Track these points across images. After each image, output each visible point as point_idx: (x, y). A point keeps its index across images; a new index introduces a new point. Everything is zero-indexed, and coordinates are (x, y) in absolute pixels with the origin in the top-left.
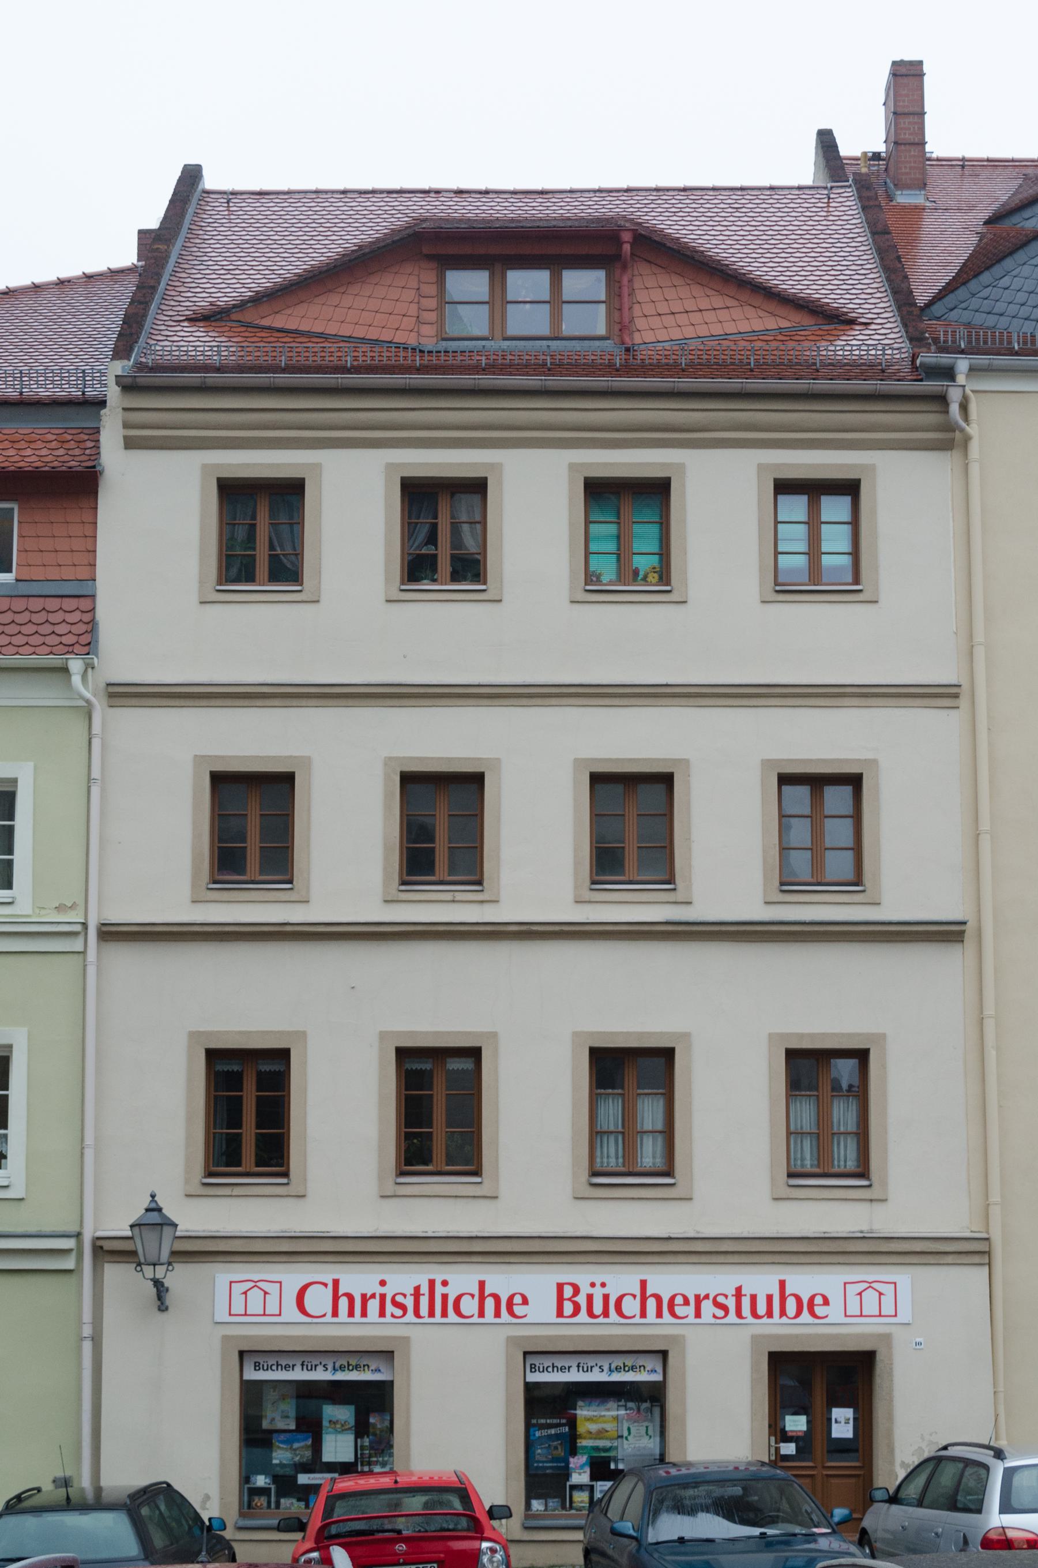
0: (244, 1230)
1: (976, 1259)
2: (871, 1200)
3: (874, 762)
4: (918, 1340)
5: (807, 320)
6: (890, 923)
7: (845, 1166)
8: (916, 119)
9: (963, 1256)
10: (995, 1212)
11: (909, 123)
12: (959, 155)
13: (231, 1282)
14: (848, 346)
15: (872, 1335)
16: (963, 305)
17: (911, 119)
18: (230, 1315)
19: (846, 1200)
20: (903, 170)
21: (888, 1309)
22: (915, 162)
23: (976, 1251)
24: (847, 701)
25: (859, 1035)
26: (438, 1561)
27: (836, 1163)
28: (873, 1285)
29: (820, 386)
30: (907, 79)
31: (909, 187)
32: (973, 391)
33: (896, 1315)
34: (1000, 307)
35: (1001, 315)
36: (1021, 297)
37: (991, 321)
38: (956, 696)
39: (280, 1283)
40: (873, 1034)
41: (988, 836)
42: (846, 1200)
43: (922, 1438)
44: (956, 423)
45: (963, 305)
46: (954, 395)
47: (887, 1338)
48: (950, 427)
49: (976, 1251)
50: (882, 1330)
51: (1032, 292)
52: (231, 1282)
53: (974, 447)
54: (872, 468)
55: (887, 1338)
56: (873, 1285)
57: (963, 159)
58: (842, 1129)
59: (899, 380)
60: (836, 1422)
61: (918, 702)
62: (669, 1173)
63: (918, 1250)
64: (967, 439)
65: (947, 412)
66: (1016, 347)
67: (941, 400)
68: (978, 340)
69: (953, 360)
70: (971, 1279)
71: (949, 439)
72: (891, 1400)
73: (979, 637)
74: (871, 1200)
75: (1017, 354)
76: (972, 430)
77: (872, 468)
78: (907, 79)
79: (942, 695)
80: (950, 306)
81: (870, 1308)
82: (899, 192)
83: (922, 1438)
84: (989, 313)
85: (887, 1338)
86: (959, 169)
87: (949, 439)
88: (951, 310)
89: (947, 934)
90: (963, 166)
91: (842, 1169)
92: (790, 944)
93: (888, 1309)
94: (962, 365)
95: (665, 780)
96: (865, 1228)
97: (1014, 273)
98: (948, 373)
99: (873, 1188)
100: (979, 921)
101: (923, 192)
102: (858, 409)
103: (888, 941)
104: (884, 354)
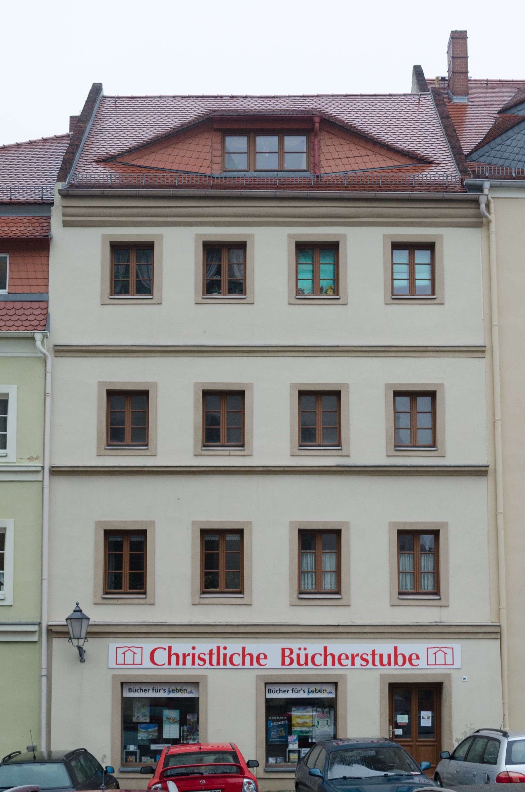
0: (123, 621)
1: (494, 636)
2: (441, 606)
3: (442, 385)
4: (464, 677)
5: (408, 162)
6: (450, 466)
7: (428, 589)
8: (463, 60)
9: (487, 634)
10: (503, 612)
11: (460, 62)
12: (485, 78)
13: (117, 648)
14: (429, 175)
15: (441, 674)
16: (487, 154)
17: (461, 60)
18: (116, 664)
19: (428, 606)
20: (457, 86)
21: (449, 661)
22: (463, 82)
23: (493, 632)
24: (428, 354)
25: (435, 523)
26: (222, 789)
27: (423, 587)
28: (441, 649)
29: (415, 195)
30: (458, 40)
31: (460, 94)
32: (492, 198)
33: (453, 664)
34: (506, 155)
35: (506, 159)
36: (516, 150)
37: (501, 162)
38: (484, 352)
39: (142, 648)
40: (441, 522)
41: (500, 422)
42: (428, 606)
43: (467, 726)
44: (484, 214)
45: (487, 154)
46: (483, 200)
47: (449, 676)
48: (481, 216)
49: (493, 632)
50: (446, 672)
51: (522, 148)
52: (117, 648)
53: (493, 226)
54: (441, 236)
55: (448, 676)
56: (441, 649)
57: (487, 81)
58: (426, 570)
59: (455, 192)
60: (423, 718)
61: (465, 354)
62: (338, 592)
63: (464, 631)
64: (489, 222)
65: (479, 208)
66: (514, 175)
67: (476, 202)
68: (494, 172)
69: (482, 182)
70: (491, 646)
71: (480, 222)
72: (451, 707)
73: (495, 322)
74: (441, 606)
75: (514, 179)
76: (492, 217)
77: (441, 236)
78: (458, 40)
79: (476, 351)
80: (481, 155)
81: (440, 660)
82: (455, 97)
83: (467, 726)
84: (500, 158)
85: (448, 676)
86: (485, 85)
87: (480, 222)
88: (481, 157)
89: (479, 472)
90: (487, 84)
91: (426, 591)
92: (399, 477)
93: (449, 661)
94: (487, 184)
95: (336, 394)
96: (437, 620)
97: (513, 138)
98: (480, 189)
99: (442, 600)
100: (495, 465)
101: (467, 97)
102: (434, 207)
103: (449, 475)
104: (447, 179)
